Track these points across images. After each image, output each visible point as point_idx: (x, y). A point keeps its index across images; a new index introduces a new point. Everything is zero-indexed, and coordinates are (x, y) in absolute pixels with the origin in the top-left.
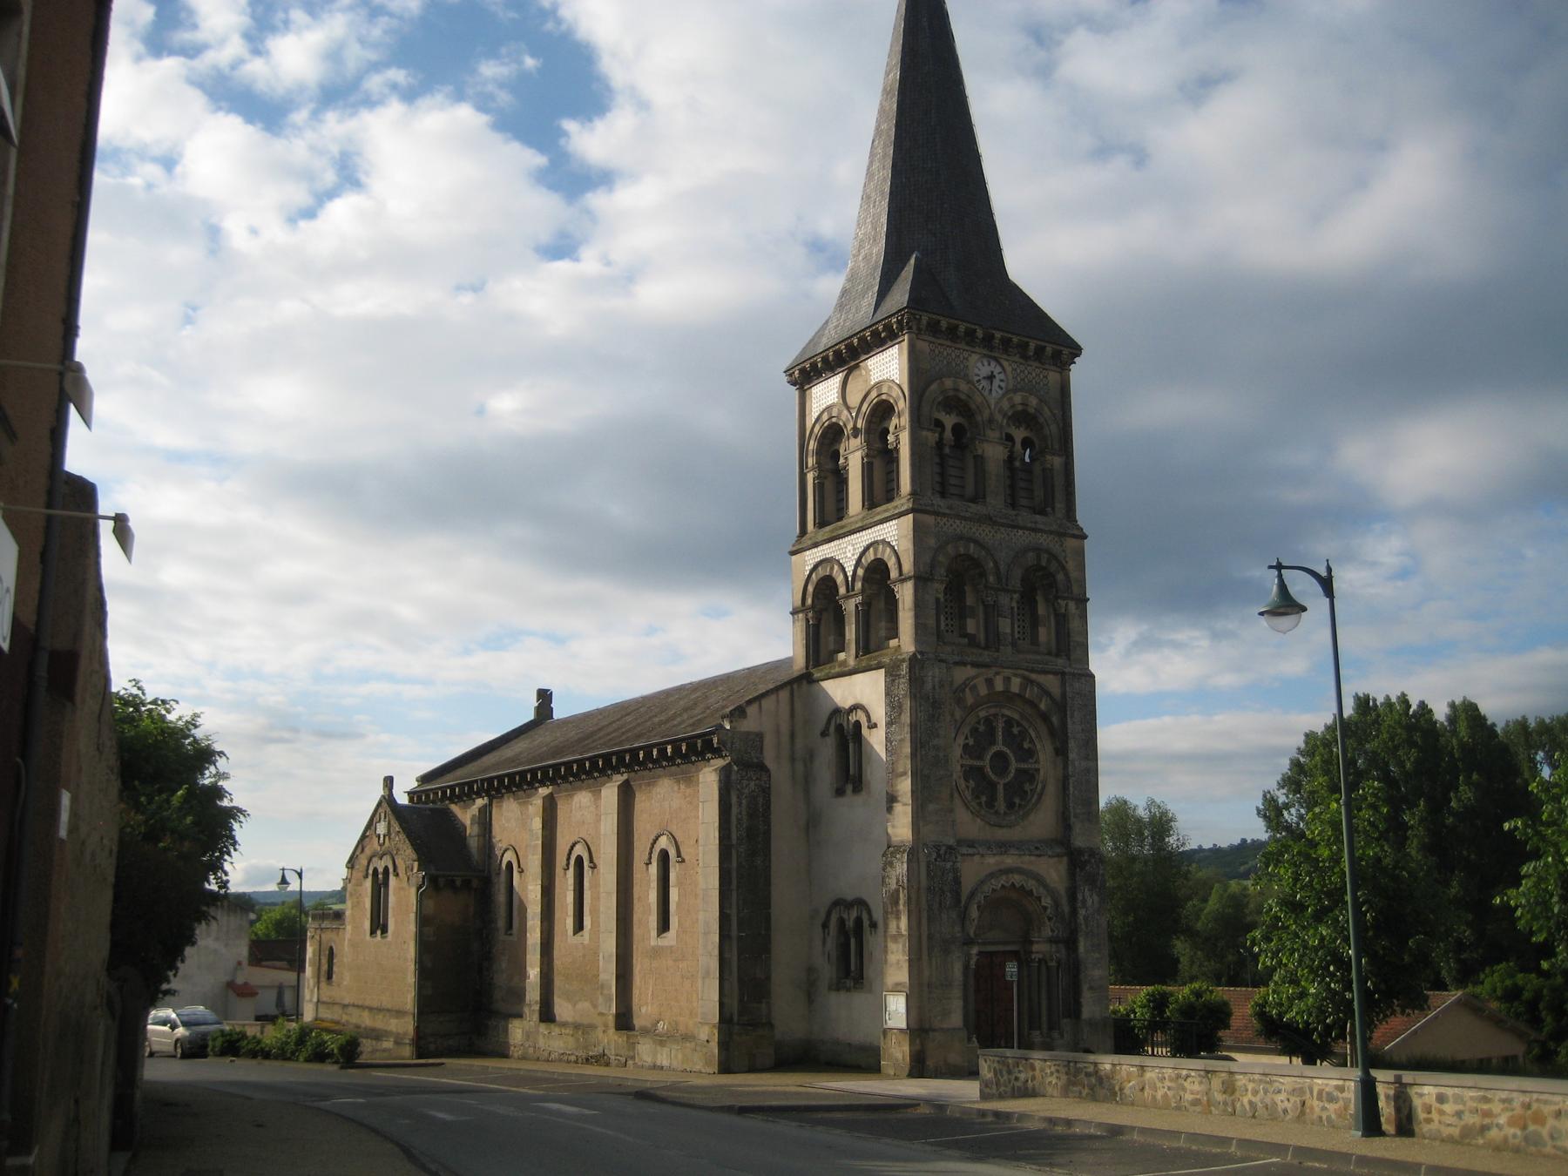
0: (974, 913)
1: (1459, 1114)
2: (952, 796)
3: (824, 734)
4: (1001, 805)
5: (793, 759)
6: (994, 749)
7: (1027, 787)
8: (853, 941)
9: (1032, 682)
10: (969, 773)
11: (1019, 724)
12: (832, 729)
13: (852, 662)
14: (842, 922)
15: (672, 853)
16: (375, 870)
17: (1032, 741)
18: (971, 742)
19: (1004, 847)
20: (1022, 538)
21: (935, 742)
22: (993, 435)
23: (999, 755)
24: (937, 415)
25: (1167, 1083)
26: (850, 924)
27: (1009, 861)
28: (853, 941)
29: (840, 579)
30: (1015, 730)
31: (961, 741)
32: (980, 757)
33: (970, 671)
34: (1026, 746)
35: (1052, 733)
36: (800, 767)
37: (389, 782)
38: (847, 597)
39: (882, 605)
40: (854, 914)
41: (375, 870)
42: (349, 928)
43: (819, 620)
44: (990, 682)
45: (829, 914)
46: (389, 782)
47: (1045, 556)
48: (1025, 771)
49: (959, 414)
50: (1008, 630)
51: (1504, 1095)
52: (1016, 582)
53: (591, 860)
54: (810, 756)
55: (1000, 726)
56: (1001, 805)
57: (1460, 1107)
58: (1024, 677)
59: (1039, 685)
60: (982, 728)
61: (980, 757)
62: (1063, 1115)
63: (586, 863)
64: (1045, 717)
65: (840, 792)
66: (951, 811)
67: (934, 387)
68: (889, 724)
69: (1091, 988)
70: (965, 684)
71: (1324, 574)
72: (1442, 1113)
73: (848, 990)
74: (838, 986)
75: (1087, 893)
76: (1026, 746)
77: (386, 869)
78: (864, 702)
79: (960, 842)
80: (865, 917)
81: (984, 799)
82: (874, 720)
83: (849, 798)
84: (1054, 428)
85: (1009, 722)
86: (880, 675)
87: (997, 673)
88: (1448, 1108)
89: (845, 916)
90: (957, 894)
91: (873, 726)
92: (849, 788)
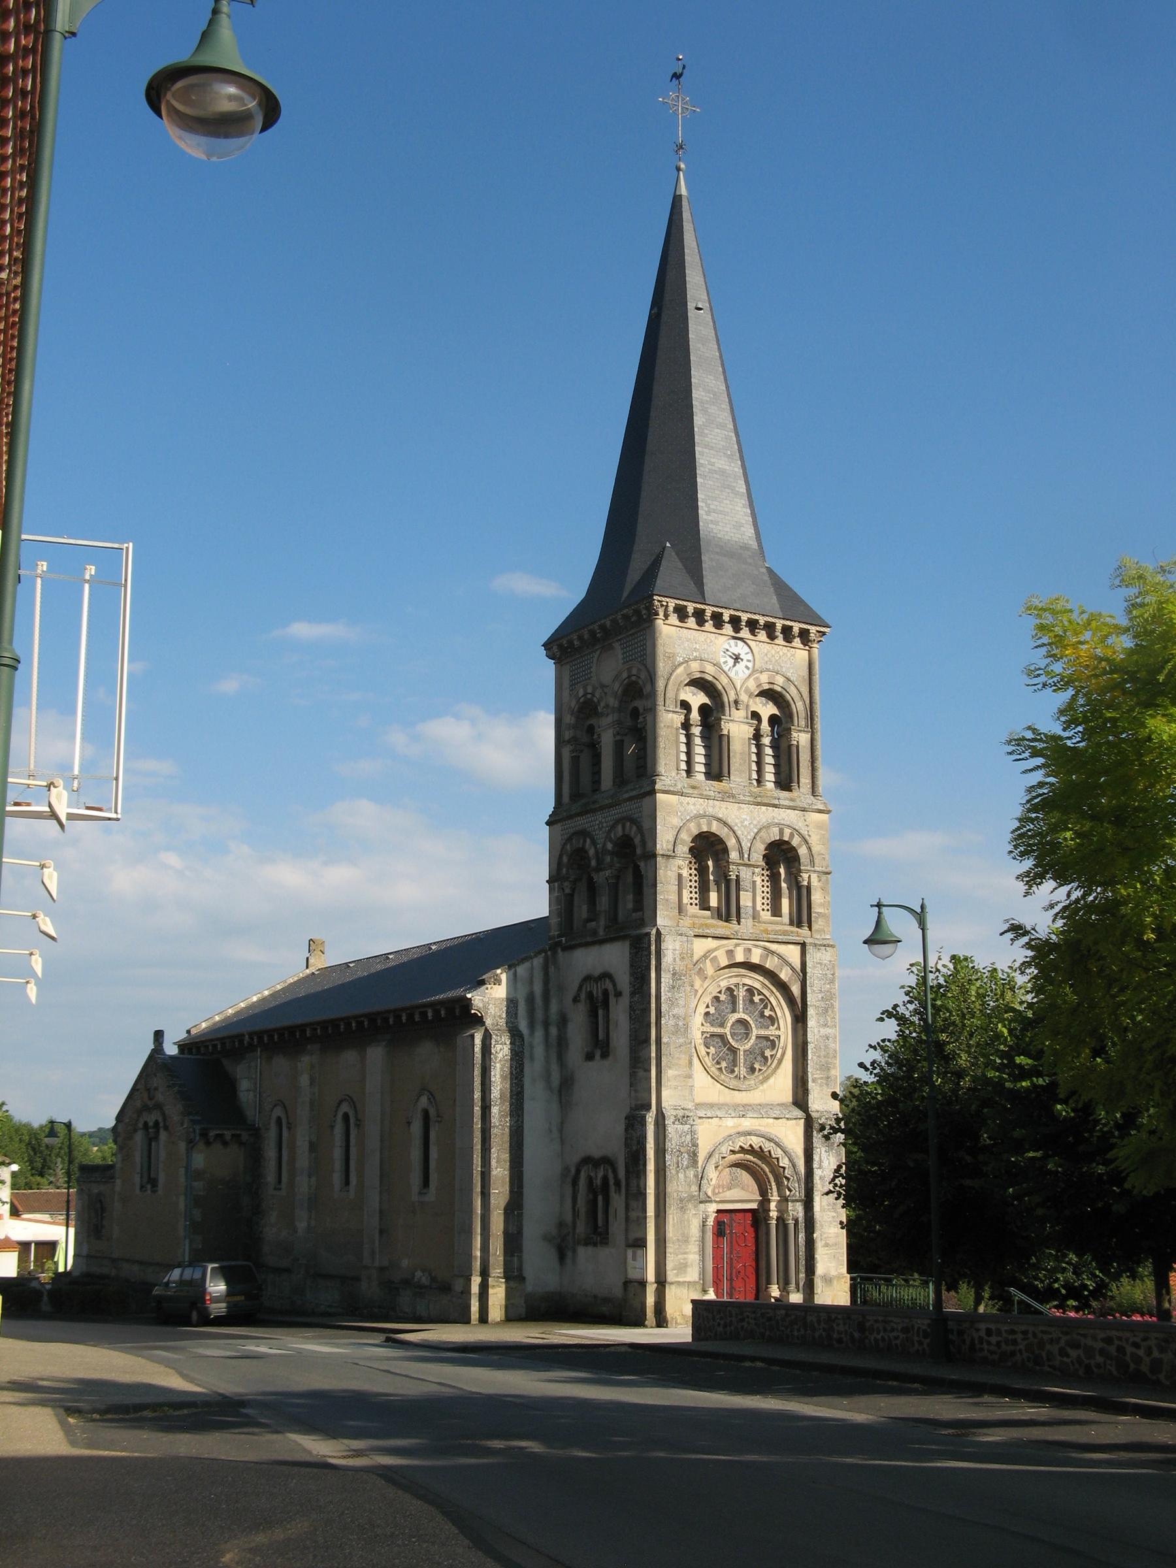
0: (712, 1173)
1: (998, 1344)
2: (691, 1063)
3: (576, 1000)
4: (742, 1070)
5: (546, 1024)
6: (736, 1016)
7: (768, 1053)
8: (600, 1198)
9: (773, 953)
10: (710, 1039)
11: (760, 993)
12: (583, 996)
13: (601, 932)
14: (590, 1180)
15: (432, 1112)
16: (146, 1124)
17: (773, 1009)
18: (712, 1010)
19: (743, 1110)
20: (766, 815)
21: (675, 1011)
22: (740, 714)
23: (742, 1022)
24: (683, 696)
25: (823, 1325)
26: (599, 1181)
27: (747, 1124)
28: (600, 1198)
29: (592, 852)
30: (756, 999)
31: (702, 1009)
32: (722, 1025)
33: (711, 943)
34: (767, 1013)
35: (790, 1000)
36: (554, 1031)
37: (159, 1035)
38: (598, 869)
39: (630, 878)
40: (601, 1174)
41: (146, 1124)
42: (118, 1182)
43: (573, 890)
44: (730, 953)
45: (578, 1171)
46: (159, 1035)
47: (787, 832)
48: (766, 1038)
49: (708, 694)
50: (750, 904)
51: (1023, 1328)
52: (758, 857)
53: (357, 1119)
54: (563, 1021)
55: (741, 994)
56: (742, 1070)
57: (999, 1339)
58: (765, 949)
59: (780, 956)
60: (723, 997)
61: (722, 1025)
62: (702, 1343)
63: (352, 1120)
64: (783, 987)
65: (589, 1057)
66: (690, 1076)
67: (680, 670)
68: (633, 994)
69: (827, 1245)
70: (705, 956)
71: (919, 910)
72: (989, 1343)
73: (595, 1245)
74: (587, 1243)
75: (824, 1155)
76: (767, 1013)
77: (157, 1124)
78: (612, 971)
79: (698, 1106)
80: (611, 1176)
81: (724, 1064)
82: (619, 988)
83: (597, 1063)
84: (800, 704)
85: (751, 991)
86: (627, 944)
87: (737, 945)
88: (994, 1339)
89: (592, 1174)
90: (694, 1156)
91: (618, 994)
92: (598, 1054)
